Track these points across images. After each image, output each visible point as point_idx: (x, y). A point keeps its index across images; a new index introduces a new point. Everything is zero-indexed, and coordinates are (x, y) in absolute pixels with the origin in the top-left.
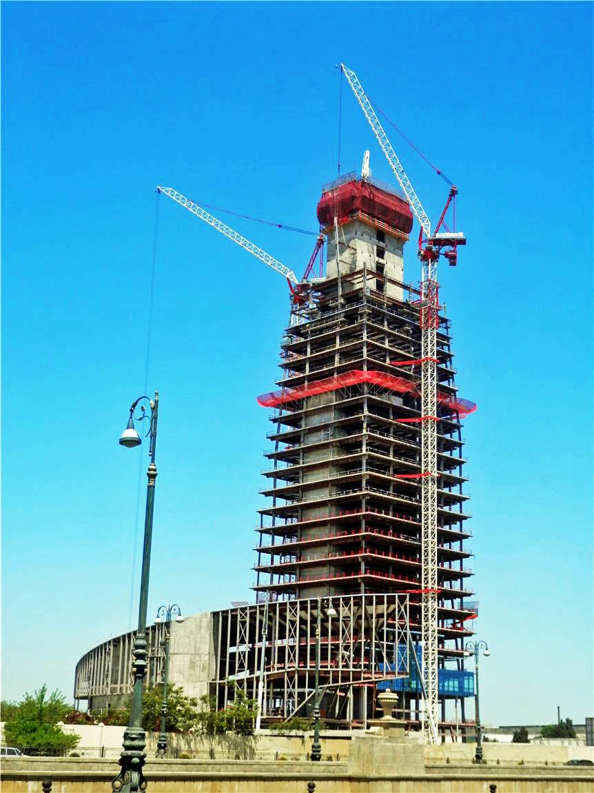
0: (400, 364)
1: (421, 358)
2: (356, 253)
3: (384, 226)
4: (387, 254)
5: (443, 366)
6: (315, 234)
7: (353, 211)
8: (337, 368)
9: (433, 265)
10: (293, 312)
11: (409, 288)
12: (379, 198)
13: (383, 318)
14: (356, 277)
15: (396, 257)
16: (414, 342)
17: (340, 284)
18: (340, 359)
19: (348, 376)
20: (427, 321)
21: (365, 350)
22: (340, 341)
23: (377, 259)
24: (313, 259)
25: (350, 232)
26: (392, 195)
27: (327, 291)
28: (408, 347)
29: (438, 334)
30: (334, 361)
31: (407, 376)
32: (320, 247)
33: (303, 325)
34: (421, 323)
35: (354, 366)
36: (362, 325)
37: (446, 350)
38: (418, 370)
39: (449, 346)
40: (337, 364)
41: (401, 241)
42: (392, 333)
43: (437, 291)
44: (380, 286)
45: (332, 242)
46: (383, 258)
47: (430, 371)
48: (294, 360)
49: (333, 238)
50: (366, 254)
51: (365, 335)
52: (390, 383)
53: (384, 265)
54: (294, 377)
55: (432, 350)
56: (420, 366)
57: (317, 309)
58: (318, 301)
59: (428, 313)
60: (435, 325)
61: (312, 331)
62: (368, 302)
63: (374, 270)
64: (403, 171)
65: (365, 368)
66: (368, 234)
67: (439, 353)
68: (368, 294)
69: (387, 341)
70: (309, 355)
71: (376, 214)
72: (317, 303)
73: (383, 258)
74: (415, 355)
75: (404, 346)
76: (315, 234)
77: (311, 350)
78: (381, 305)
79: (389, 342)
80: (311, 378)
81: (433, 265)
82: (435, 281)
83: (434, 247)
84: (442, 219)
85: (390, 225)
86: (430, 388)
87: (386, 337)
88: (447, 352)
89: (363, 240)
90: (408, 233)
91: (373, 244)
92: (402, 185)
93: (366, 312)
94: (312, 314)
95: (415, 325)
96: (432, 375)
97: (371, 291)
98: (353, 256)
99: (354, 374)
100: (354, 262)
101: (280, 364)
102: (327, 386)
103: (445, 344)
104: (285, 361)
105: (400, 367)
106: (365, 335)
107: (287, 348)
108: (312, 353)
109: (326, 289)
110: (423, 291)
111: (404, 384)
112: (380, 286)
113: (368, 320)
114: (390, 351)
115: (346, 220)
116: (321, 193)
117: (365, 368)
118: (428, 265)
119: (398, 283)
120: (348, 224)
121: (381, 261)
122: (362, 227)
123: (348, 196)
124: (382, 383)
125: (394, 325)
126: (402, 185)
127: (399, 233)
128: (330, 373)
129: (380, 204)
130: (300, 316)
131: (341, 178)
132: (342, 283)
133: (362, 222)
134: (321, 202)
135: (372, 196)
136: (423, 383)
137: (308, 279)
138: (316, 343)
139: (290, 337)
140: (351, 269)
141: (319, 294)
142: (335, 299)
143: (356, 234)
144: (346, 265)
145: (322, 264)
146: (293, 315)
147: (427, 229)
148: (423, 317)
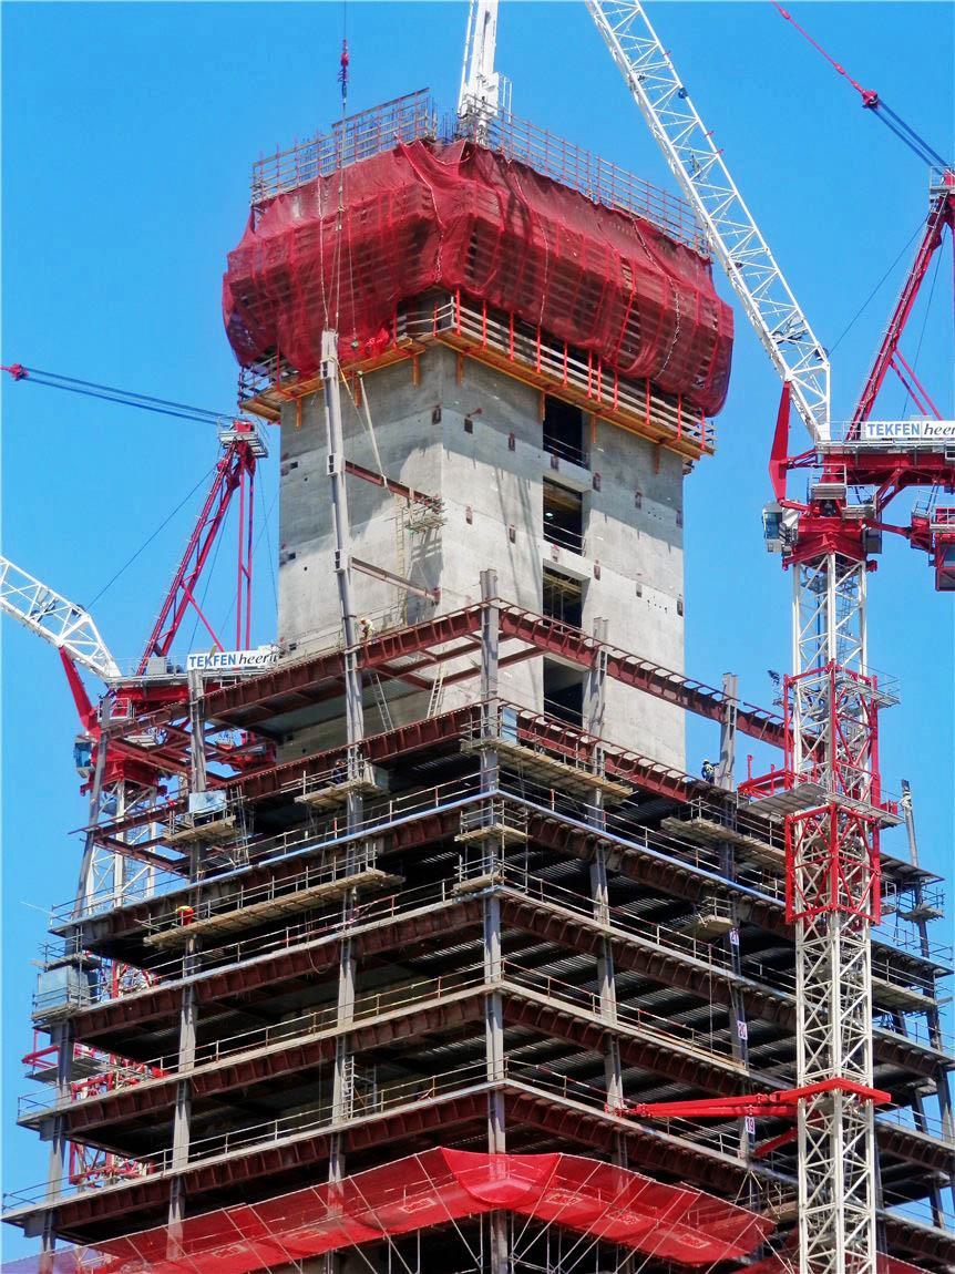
0: (680, 1111)
1: (791, 1077)
2: (436, 523)
3: (583, 383)
4: (597, 526)
5: (902, 1120)
6: (206, 416)
7: (417, 302)
8: (345, 1134)
9: (848, 588)
10: (101, 836)
11: (723, 707)
12: (554, 228)
13: (589, 863)
14: (438, 649)
15: (645, 539)
16: (749, 996)
17: (353, 686)
18: (360, 1087)
19: (407, 1182)
20: (821, 881)
21: (495, 1038)
22: (360, 990)
23: (546, 550)
24: (200, 551)
25: (401, 411)
26: (625, 218)
27: (275, 722)
28: (722, 1021)
29: (880, 954)
30: (328, 1094)
31: (722, 1180)
32: (234, 483)
33: (152, 907)
34: (788, 893)
35: (438, 1125)
36: (475, 905)
37: (915, 1031)
38: (778, 1135)
39: (932, 1014)
40: (342, 1117)
41: (669, 454)
42: (635, 950)
43: (872, 724)
44: (564, 695)
45: (305, 461)
46: (574, 543)
47: (840, 1149)
48: (103, 1094)
49: (319, 438)
50: (490, 529)
51: (494, 960)
52: (631, 1220)
53: (580, 583)
54: (104, 1187)
55: (851, 1038)
56: (787, 1125)
57: (229, 820)
58: (226, 771)
59: (827, 841)
60: (864, 904)
61: (207, 940)
62: (507, 778)
63: (535, 614)
64: (682, 94)
65: (497, 1138)
66: (500, 423)
67: (884, 1049)
68: (510, 741)
69: (608, 993)
70: (187, 1067)
71: (539, 313)
72: (229, 786)
73: (574, 543)
74: (757, 1063)
75: (699, 1012)
76: (206, 416)
77: (203, 1036)
78: (575, 799)
79: (621, 995)
80: (202, 1194)
81: (848, 588)
82: (863, 670)
83: (850, 494)
84: (892, 343)
85: (615, 371)
86: (842, 1240)
87: (605, 967)
88: (925, 1045)
89: (475, 455)
90: (709, 413)
91: (524, 474)
92: (677, 164)
93: (495, 835)
94: (198, 849)
95: (752, 903)
96: (853, 1172)
97: (523, 723)
98: (418, 539)
99: (439, 1168)
100: (428, 567)
101: (30, 1113)
102: (292, 1235)
103: (912, 1006)
104: (52, 1098)
105: (677, 1128)
106: (494, 960)
107: (68, 1028)
108: (203, 1054)
109: (277, 709)
110: (798, 726)
111: (706, 1219)
112: (564, 695)
113: (512, 878)
114: (627, 1043)
115: (382, 348)
116: (244, 200)
117: (497, 1138)
118: (820, 586)
119: (665, 683)
120: (391, 368)
121: (568, 561)
122: (466, 383)
123: (392, 217)
124: (592, 1216)
125: (647, 904)
126: (677, 164)
127: (665, 418)
128: (306, 1167)
129: (562, 267)
130: (139, 851)
131: (354, 123)
132: (366, 682)
133: (466, 358)
134: (244, 255)
135: (517, 221)
136: (804, 1214)
137: (173, 655)
138: (229, 1003)
139: (87, 967)
140: (413, 607)
141: (235, 737)
142: (328, 763)
143: (436, 419)
144: (380, 585)
145: (245, 572)
146: (96, 851)
147: (812, 399)
148: (799, 860)
